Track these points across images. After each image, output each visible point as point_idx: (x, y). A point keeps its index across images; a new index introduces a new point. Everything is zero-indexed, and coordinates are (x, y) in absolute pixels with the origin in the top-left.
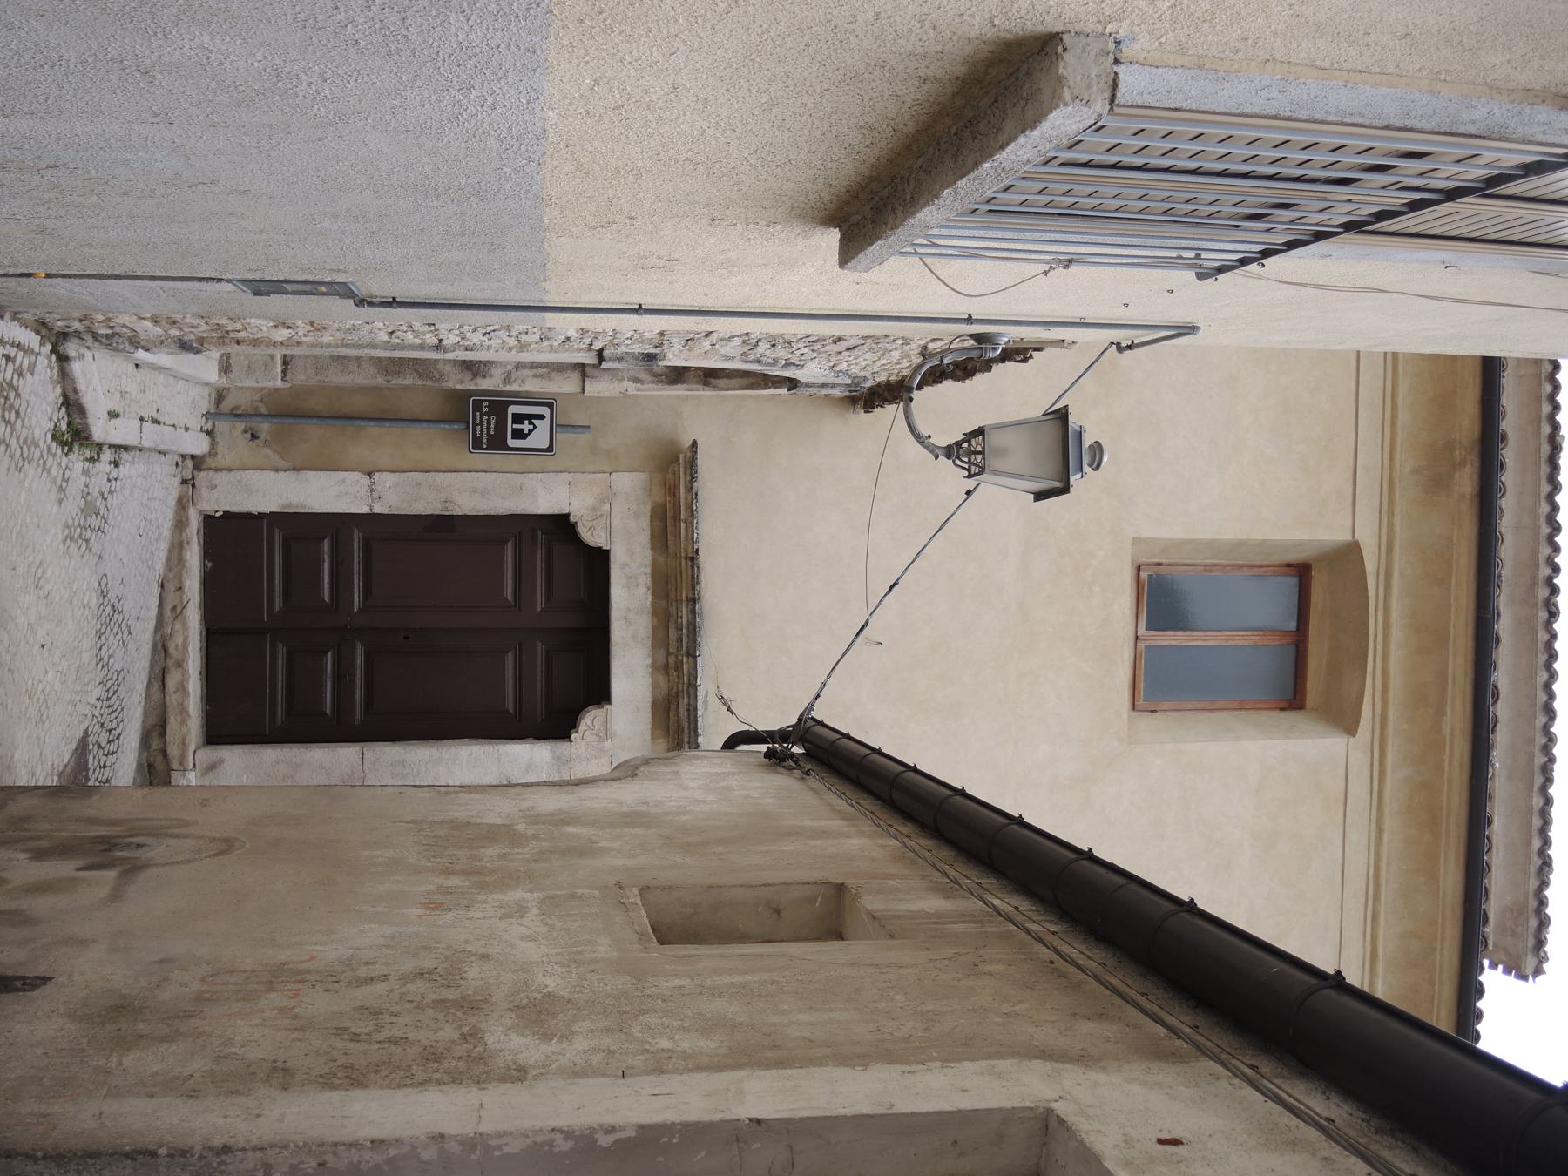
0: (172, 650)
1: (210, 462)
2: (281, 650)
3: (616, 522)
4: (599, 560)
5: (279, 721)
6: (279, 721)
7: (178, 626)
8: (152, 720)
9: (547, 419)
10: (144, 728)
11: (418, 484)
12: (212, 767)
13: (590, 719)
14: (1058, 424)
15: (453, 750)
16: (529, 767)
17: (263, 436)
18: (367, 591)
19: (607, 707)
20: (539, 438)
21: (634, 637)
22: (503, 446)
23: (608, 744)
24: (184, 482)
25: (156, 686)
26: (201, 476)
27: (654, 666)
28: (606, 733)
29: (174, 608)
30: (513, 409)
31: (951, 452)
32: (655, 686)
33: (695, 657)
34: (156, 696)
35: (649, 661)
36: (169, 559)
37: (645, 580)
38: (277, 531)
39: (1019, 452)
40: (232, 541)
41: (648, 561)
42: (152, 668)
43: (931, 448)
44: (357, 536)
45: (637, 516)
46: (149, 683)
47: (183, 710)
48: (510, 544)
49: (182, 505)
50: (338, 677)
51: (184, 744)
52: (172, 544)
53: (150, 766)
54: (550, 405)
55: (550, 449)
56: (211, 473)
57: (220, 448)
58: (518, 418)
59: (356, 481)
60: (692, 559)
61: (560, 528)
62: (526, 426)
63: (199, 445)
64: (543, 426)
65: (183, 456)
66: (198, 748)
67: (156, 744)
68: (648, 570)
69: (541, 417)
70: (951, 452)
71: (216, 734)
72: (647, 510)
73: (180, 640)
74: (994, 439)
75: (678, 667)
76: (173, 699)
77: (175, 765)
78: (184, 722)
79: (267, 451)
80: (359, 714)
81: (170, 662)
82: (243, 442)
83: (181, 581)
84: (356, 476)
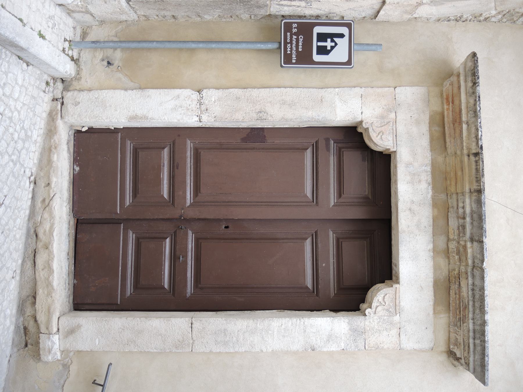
0: (41, 235)
1: (75, 83)
2: (131, 236)
3: (401, 128)
5: (128, 293)
6: (128, 293)
7: (46, 215)
8: (27, 292)
9: (347, 38)
10: (20, 298)
11: (238, 98)
12: (71, 332)
13: (381, 296)
15: (266, 322)
16: (330, 338)
17: (116, 63)
18: (197, 190)
19: (395, 286)
20: (340, 53)
21: (418, 226)
23: (397, 318)
24: (55, 100)
25: (29, 264)
26: (69, 96)
27: (435, 250)
28: (396, 308)
29: (44, 200)
30: (317, 30)
32: (436, 268)
33: (481, 242)
34: (29, 272)
35: (431, 246)
36: (40, 160)
37: (426, 177)
38: (129, 142)
40: (93, 146)
41: (428, 161)
42: (26, 248)
44: (189, 145)
45: (418, 122)
46: (24, 261)
47: (49, 284)
48: (168, 240)
49: (52, 117)
50: (174, 258)
51: (49, 313)
52: (44, 149)
53: (25, 328)
54: (349, 26)
55: (349, 62)
56: (76, 93)
57: (84, 73)
58: (322, 37)
59: (187, 96)
60: (477, 154)
62: (329, 44)
63: (67, 68)
64: (343, 43)
65: (55, 79)
66: (63, 314)
67: (29, 311)
68: (429, 169)
69: (341, 36)
71: (84, 301)
72: (426, 118)
73: (47, 226)
75: (461, 252)
76: (41, 274)
77: (43, 329)
78: (49, 294)
79: (120, 75)
80: (190, 289)
81: (40, 245)
82: (101, 68)
83: (49, 178)
84: (187, 92)
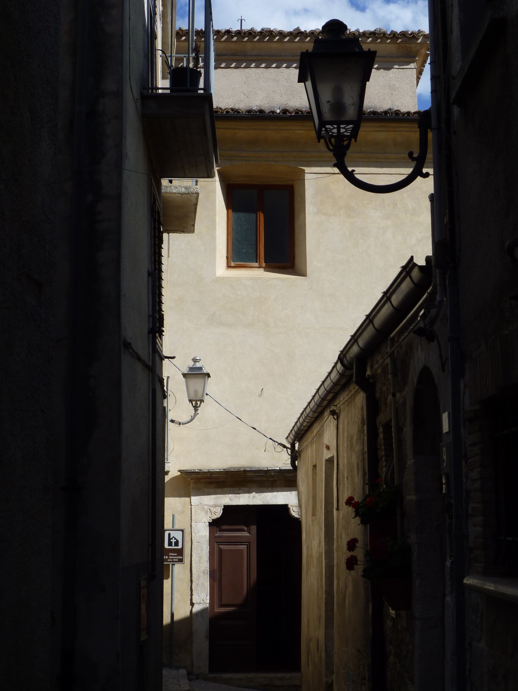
4: (227, 509)
11: (197, 585)
14: (187, 376)
19: (289, 506)
20: (178, 535)
22: (182, 549)
31: (196, 408)
39: (196, 383)
43: (195, 415)
55: (182, 531)
58: (170, 544)
61: (215, 525)
62: (173, 541)
63: (183, 672)
64: (173, 534)
69: (169, 534)
70: (196, 408)
74: (193, 397)
